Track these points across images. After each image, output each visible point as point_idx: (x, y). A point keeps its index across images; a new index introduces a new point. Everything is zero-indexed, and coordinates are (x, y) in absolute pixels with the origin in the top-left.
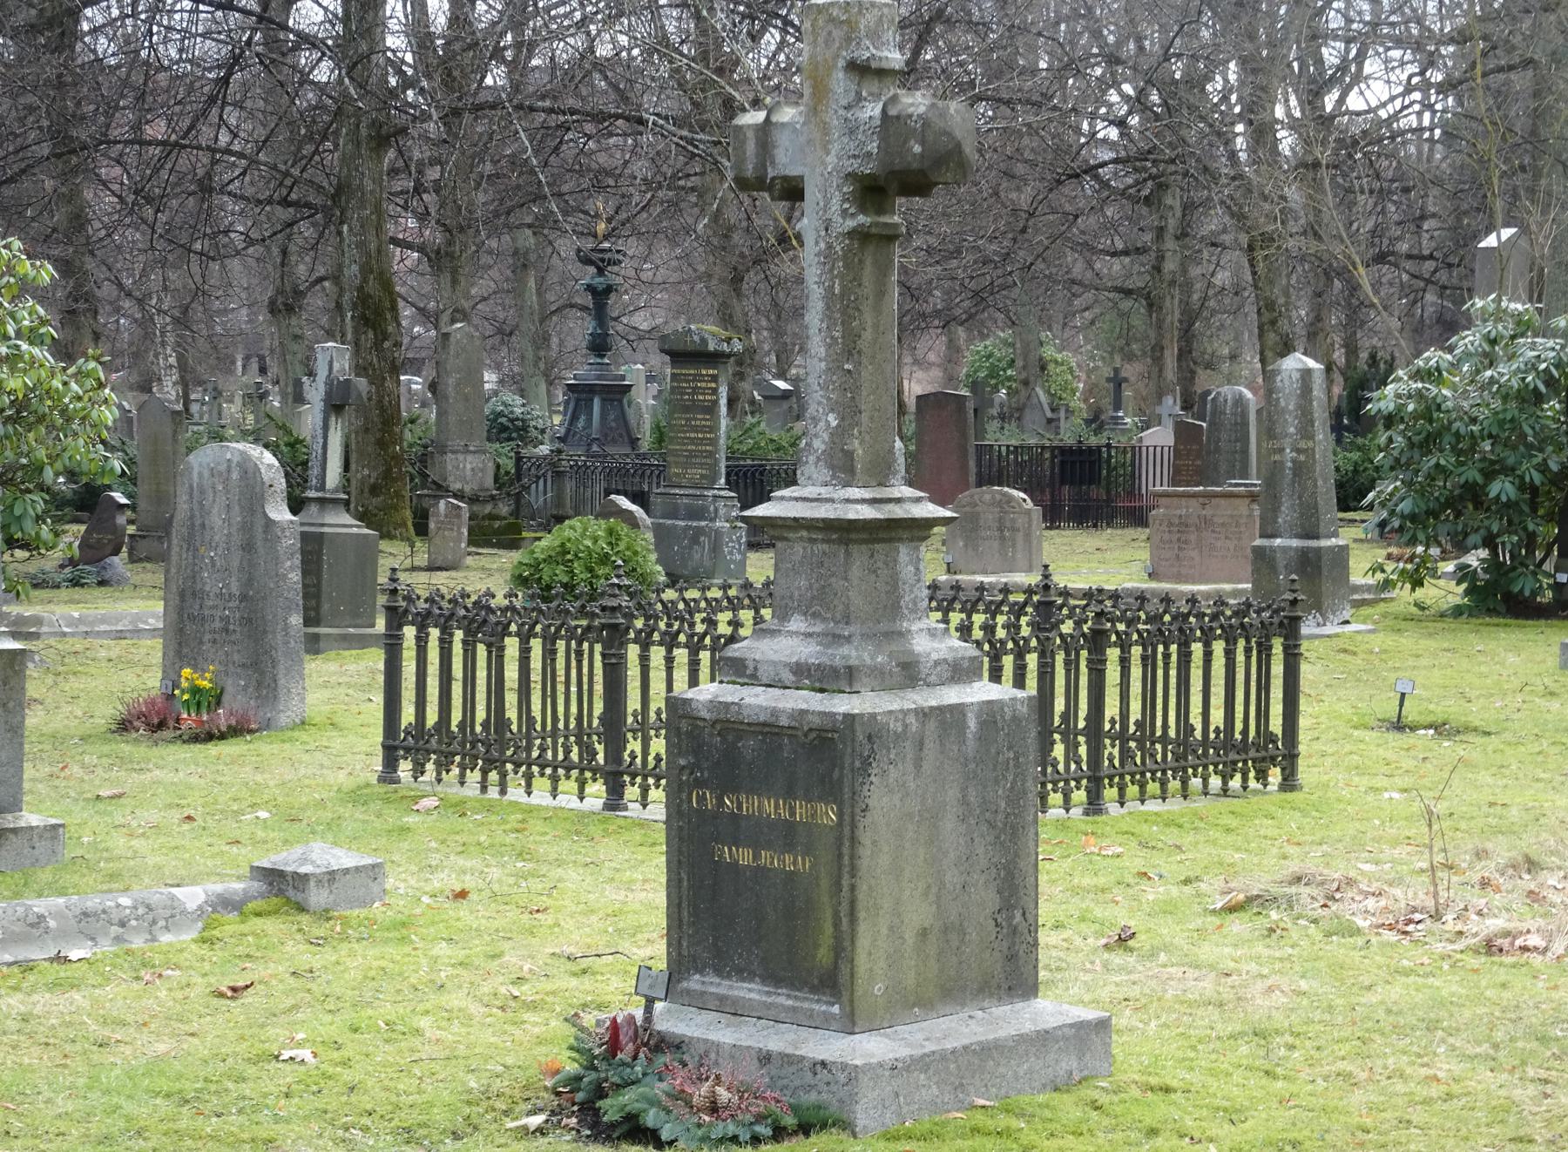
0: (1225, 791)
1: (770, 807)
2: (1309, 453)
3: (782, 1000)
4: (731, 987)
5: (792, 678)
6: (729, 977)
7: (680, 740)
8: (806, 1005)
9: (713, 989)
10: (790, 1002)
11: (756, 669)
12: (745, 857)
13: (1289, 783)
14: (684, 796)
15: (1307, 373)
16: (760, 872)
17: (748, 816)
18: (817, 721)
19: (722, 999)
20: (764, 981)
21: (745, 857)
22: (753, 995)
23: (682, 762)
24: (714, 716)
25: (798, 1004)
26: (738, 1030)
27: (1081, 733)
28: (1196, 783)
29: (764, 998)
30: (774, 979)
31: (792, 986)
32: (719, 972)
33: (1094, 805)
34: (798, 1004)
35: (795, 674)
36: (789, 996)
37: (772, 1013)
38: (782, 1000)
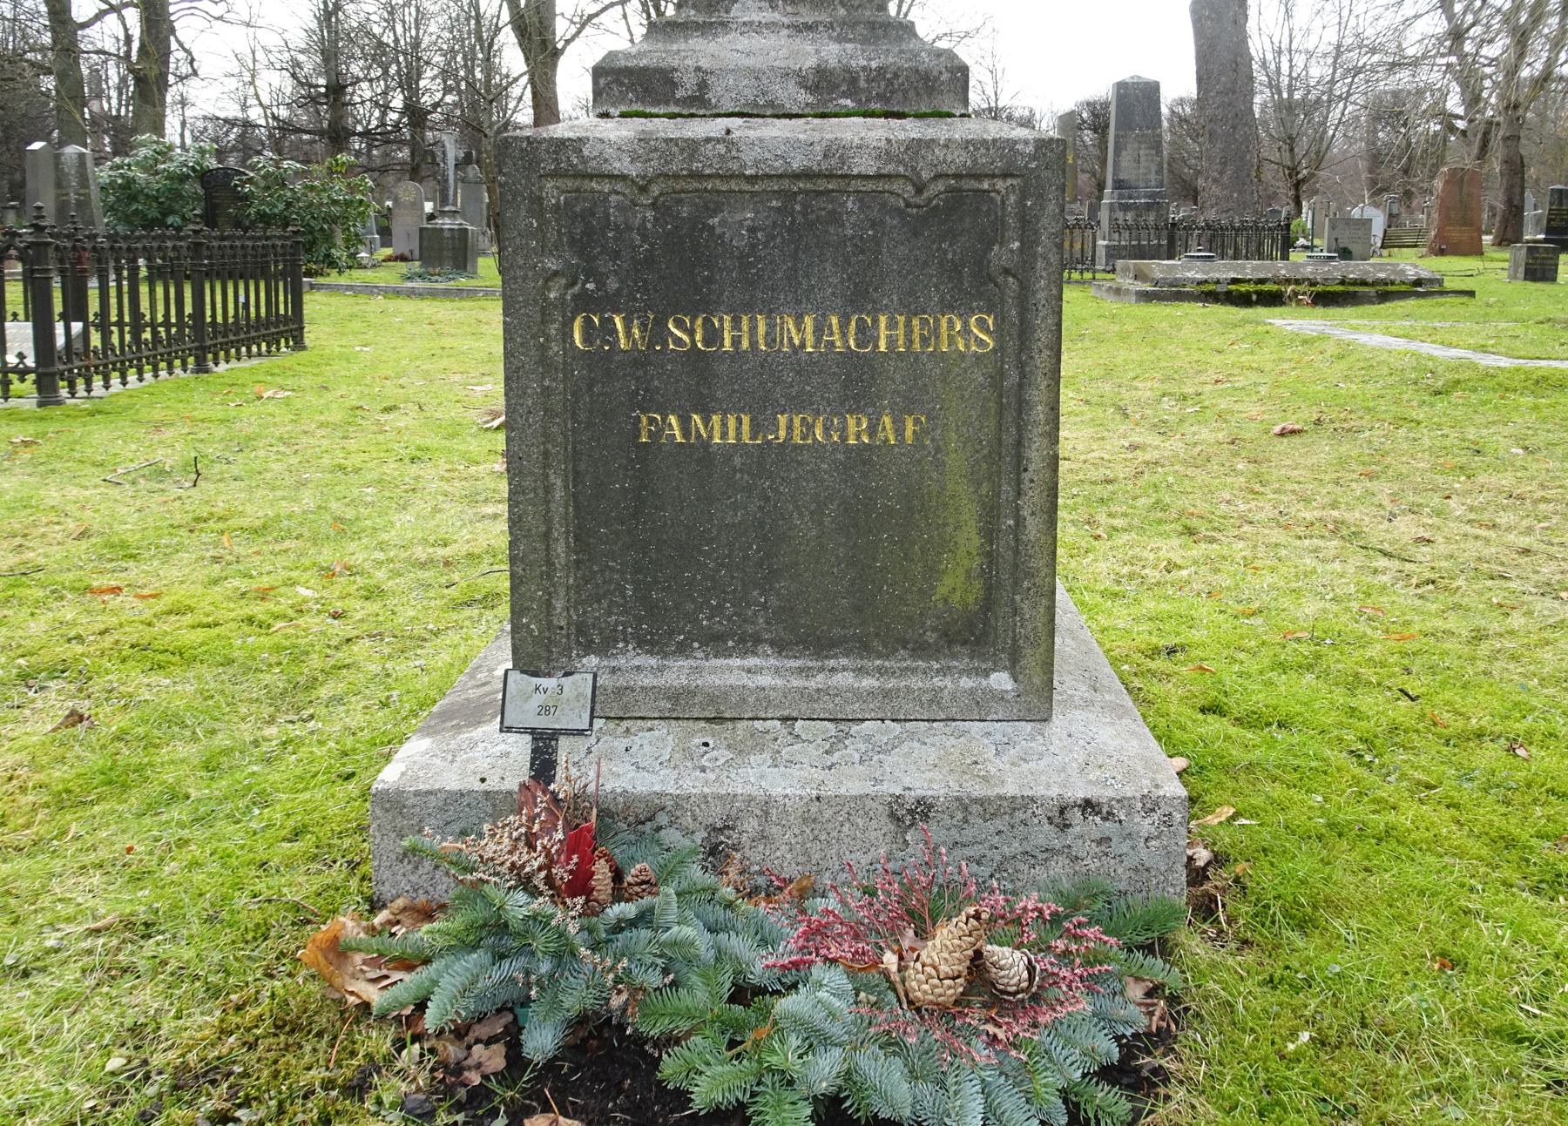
0: (269, 352)
1: (799, 332)
2: (87, 196)
3: (844, 680)
4: (697, 670)
5: (804, 97)
6: (683, 650)
7: (543, 223)
8: (916, 682)
9: (648, 681)
10: (868, 683)
11: (703, 86)
12: (726, 430)
13: (299, 344)
14: (553, 329)
15: (81, 156)
16: (769, 460)
17: (737, 354)
18: (960, 159)
19: (678, 697)
20: (781, 647)
21: (726, 430)
22: (765, 680)
23: (552, 264)
24: (654, 166)
25: (892, 683)
26: (784, 761)
27: (114, 324)
28: (254, 349)
29: (797, 682)
30: (810, 639)
31: (863, 648)
32: (648, 644)
33: (201, 368)
34: (892, 683)
35: (814, 89)
36: (860, 671)
37: (826, 706)
38: (844, 680)
